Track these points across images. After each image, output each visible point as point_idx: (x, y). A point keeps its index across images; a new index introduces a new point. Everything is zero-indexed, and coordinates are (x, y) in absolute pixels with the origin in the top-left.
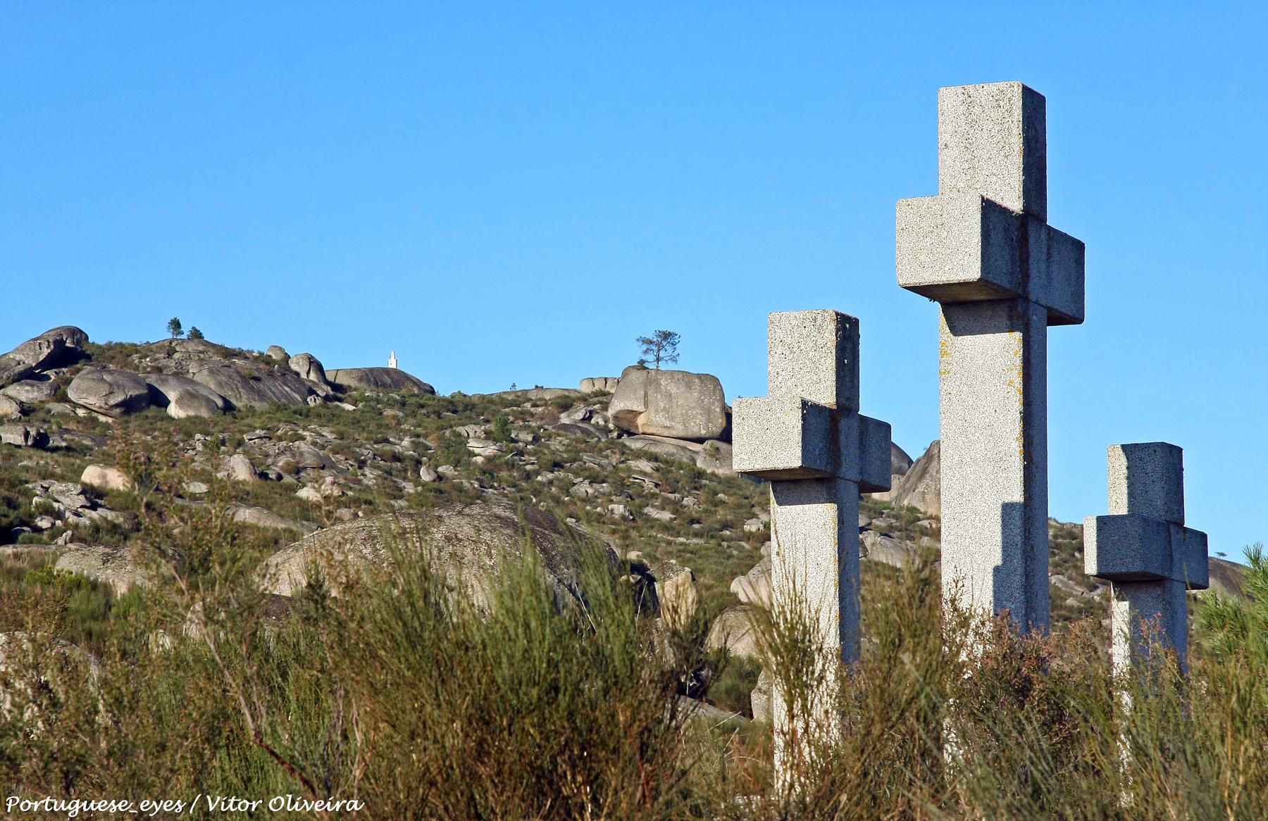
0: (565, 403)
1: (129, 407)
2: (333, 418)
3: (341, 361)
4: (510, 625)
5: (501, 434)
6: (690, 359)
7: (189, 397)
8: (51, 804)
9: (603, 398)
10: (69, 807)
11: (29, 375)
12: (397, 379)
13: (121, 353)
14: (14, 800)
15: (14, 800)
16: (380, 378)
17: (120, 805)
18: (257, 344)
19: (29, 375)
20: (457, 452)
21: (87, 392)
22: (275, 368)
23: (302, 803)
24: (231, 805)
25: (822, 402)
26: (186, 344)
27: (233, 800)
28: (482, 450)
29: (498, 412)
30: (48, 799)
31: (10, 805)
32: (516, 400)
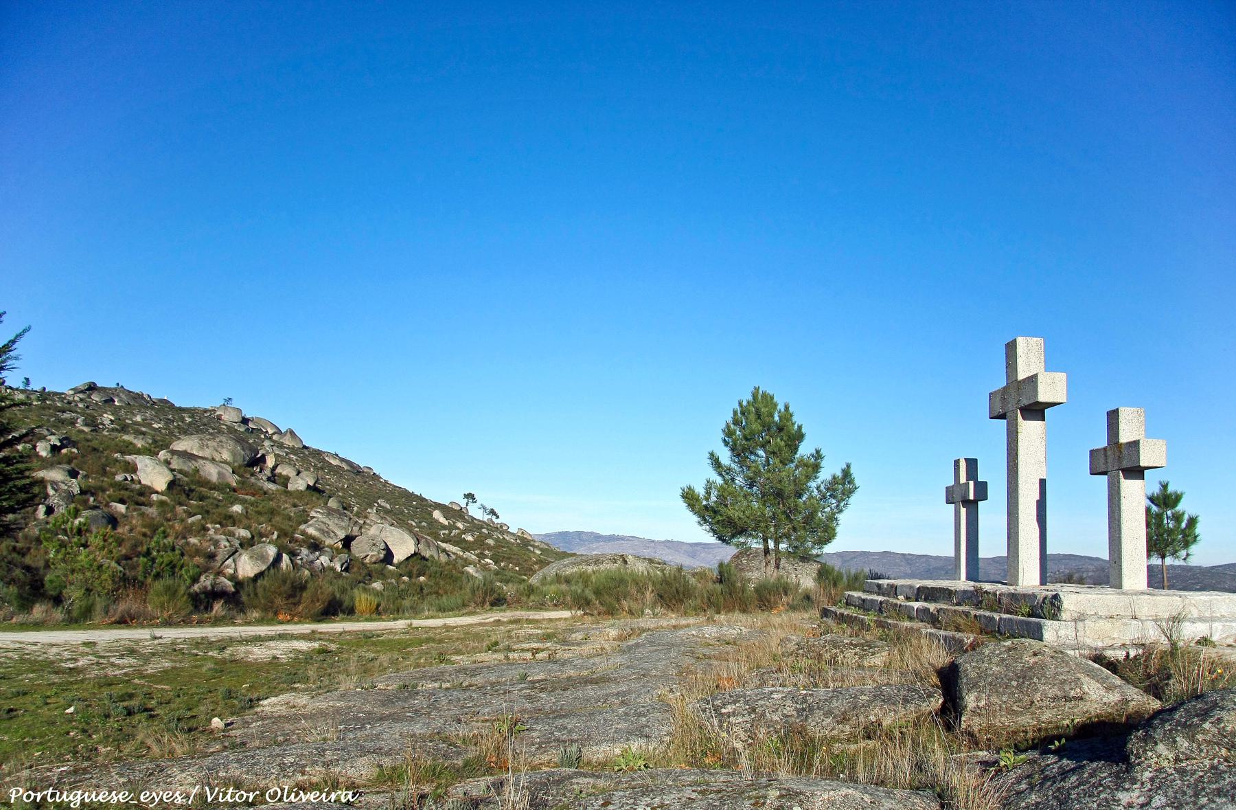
0: (206, 411)
1: (106, 401)
2: (153, 409)
3: (155, 396)
4: (691, 726)
5: (192, 417)
6: (235, 404)
7: (120, 401)
8: (53, 795)
9: (214, 411)
10: (71, 798)
11: (82, 392)
12: (166, 402)
13: (104, 389)
14: (18, 791)
15: (18, 791)
16: (162, 401)
17: (120, 796)
18: (137, 391)
19: (82, 392)
20: (183, 420)
21: (96, 397)
22: (139, 397)
23: (297, 795)
24: (228, 796)
25: (1142, 458)
26: (120, 389)
27: (231, 791)
28: (188, 420)
29: (192, 412)
30: (51, 790)
31: (13, 796)
32: (195, 409)
